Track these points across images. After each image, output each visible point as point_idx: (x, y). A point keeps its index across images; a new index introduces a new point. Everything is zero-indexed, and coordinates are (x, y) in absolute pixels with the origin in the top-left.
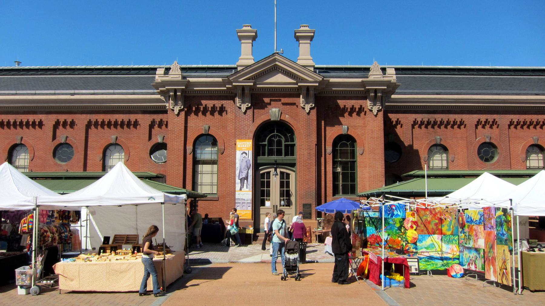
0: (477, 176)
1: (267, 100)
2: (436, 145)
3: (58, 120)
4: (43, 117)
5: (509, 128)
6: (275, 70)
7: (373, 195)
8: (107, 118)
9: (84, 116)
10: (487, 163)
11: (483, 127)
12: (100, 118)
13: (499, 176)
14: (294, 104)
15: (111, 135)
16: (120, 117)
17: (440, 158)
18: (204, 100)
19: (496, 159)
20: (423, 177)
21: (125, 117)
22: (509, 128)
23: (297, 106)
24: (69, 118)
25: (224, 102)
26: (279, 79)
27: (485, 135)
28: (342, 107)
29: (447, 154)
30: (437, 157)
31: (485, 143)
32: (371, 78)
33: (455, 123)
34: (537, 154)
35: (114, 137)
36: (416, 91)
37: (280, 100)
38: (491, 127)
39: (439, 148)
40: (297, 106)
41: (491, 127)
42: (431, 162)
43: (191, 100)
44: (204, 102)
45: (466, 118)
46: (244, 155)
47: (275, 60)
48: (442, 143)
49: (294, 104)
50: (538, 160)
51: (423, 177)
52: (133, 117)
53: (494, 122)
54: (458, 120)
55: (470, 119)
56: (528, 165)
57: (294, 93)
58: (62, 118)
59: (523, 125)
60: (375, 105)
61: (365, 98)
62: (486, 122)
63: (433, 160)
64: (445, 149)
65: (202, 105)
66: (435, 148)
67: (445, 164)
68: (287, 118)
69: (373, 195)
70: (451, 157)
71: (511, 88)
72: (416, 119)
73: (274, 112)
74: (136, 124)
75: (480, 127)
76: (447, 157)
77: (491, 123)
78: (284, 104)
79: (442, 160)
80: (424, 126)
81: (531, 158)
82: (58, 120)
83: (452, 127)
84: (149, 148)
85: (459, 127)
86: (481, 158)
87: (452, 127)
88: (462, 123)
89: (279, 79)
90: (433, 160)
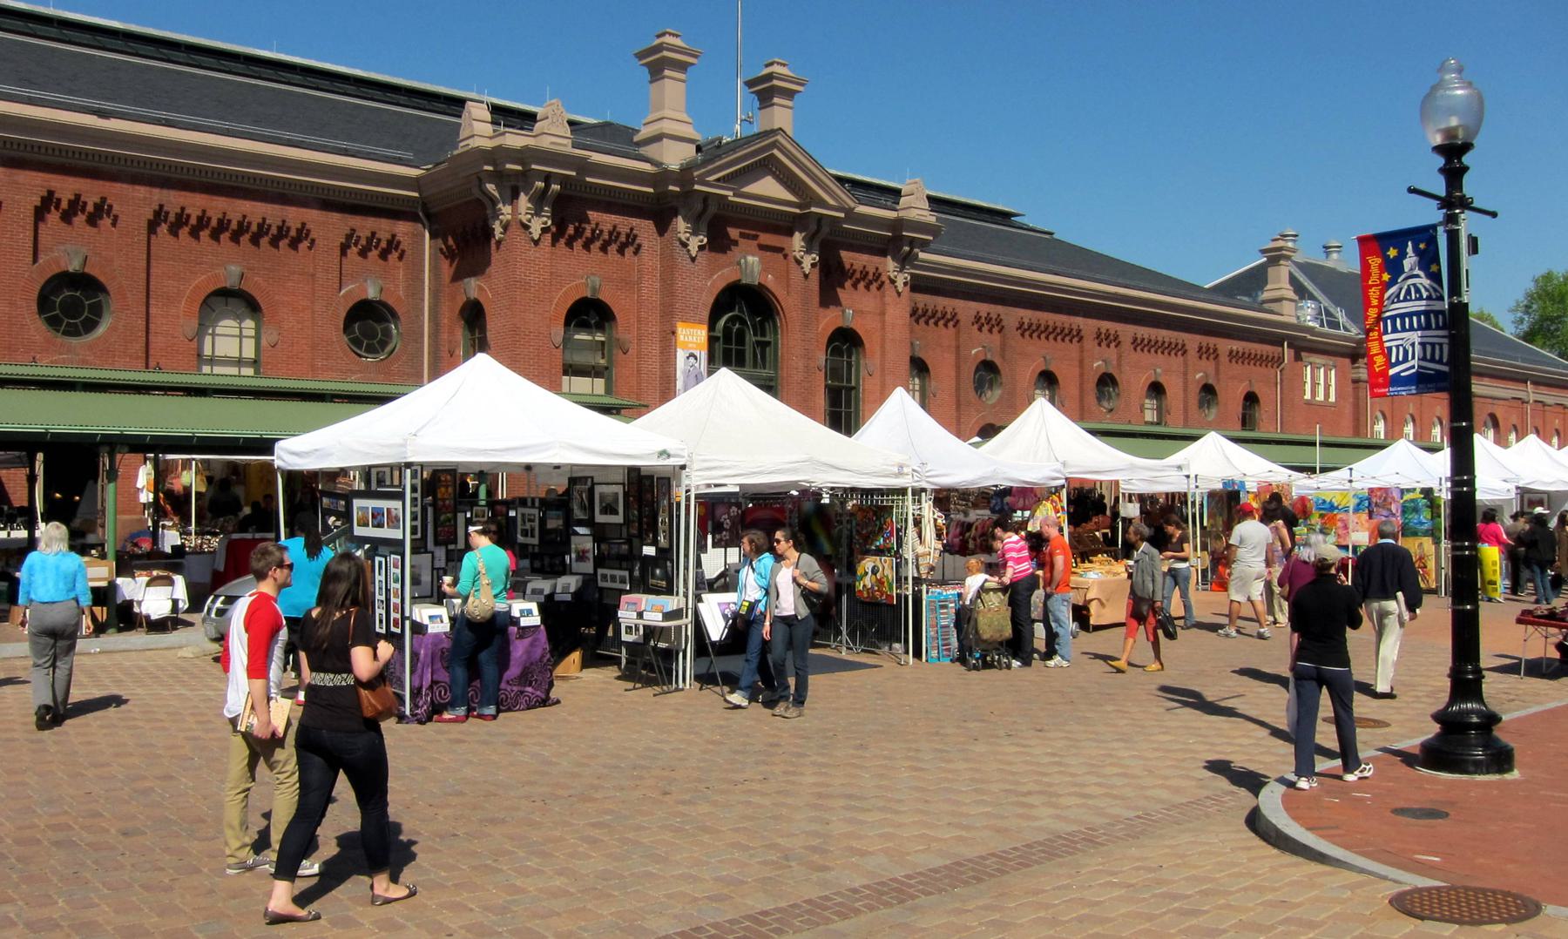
0: (1194, 438)
1: (734, 233)
2: (224, 294)
3: (51, 193)
4: (313, 216)
6: (768, 167)
8: (217, 206)
9: (141, 191)
10: (74, 341)
11: (363, 253)
12: (195, 203)
13: (1094, 432)
14: (779, 250)
15: (229, 265)
16: (255, 211)
17: (237, 332)
18: (597, 210)
19: (101, 330)
20: (1314, 444)
21: (272, 213)
23: (785, 256)
24: (91, 190)
25: (635, 222)
26: (768, 188)
27: (69, 249)
28: (847, 266)
29: (922, 379)
30: (227, 326)
32: (545, 143)
33: (282, 231)
35: (235, 269)
36: (287, 135)
37: (755, 237)
40: (785, 256)
42: (208, 340)
43: (573, 206)
44: (593, 215)
45: (118, 193)
46: (692, 360)
47: (774, 145)
48: (244, 287)
49: (779, 250)
51: (1314, 444)
52: (294, 216)
54: (294, 225)
55: (966, 309)
56: (207, 351)
57: (783, 225)
58: (66, 187)
60: (538, 213)
61: (883, 253)
64: (252, 306)
65: (589, 222)
66: (222, 299)
67: (249, 352)
68: (769, 280)
72: (183, 209)
73: (751, 264)
74: (300, 237)
75: (53, 217)
76: (258, 330)
78: (762, 247)
79: (241, 336)
80: (286, 241)
81: (218, 330)
82: (51, 193)
83: (195, 233)
84: (344, 314)
86: (53, 322)
87: (195, 233)
88: (302, 234)
89: (768, 188)
90: (214, 335)
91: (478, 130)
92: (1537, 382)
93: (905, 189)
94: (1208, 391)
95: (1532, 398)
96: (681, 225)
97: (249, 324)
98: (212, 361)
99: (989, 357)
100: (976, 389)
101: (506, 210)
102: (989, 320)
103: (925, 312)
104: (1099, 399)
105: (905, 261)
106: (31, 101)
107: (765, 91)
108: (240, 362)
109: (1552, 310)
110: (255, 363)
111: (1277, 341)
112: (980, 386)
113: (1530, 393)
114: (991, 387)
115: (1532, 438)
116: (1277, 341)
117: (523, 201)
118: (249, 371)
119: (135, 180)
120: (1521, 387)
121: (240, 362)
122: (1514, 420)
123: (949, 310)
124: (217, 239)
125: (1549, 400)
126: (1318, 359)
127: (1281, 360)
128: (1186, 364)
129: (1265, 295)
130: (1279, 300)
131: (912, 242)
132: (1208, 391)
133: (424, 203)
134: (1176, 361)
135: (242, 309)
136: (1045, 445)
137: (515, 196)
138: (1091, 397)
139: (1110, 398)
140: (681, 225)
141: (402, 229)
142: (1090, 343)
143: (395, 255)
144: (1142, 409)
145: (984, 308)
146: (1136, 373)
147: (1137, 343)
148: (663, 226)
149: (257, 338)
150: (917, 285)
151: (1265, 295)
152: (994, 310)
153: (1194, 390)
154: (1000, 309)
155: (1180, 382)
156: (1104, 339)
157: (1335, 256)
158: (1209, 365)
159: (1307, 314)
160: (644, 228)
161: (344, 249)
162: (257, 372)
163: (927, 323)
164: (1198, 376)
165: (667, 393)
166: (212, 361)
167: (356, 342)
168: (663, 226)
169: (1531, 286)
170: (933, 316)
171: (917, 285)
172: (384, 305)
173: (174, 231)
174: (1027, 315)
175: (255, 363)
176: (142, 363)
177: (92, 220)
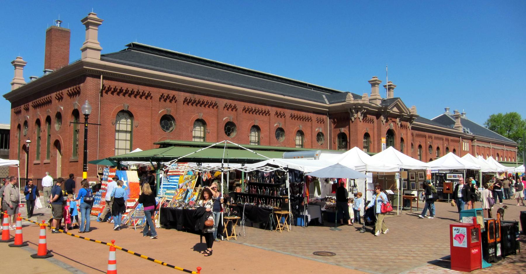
2: (123, 111)
5: (160, 101)
7: (38, 149)
9: (182, 94)
14: (394, 122)
16: (131, 87)
22: (160, 101)
30: (123, 121)
31: (279, 128)
34: (126, 119)
35: (126, 105)
38: (171, 101)
39: (125, 114)
41: (171, 101)
42: (118, 125)
44: (368, 116)
47: (398, 101)
50: (127, 124)
53: (149, 95)
56: (194, 135)
59: (115, 91)
61: (407, 121)
62: (168, 97)
63: (119, 124)
64: (130, 115)
69: (38, 149)
70: (135, 122)
71: (186, 71)
73: (392, 126)
74: (148, 96)
77: (171, 98)
81: (121, 122)
83: (141, 97)
85: (146, 98)
88: (174, 98)
90: (119, 124)
91: (350, 100)
92: (507, 145)
93: (363, 96)
94: (447, 148)
95: (492, 147)
96: (382, 118)
97: (129, 120)
98: (194, 137)
99: (280, 126)
100: (277, 137)
101: (356, 115)
102: (280, 114)
103: (248, 109)
104: (318, 141)
105: (411, 123)
106: (134, 66)
107: (390, 88)
108: (200, 138)
109: (494, 124)
110: (204, 138)
111: (459, 137)
112: (278, 136)
113: (505, 148)
114: (282, 136)
115: (491, 158)
116: (459, 137)
117: (359, 113)
118: (256, 144)
119: (288, 108)
120: (488, 144)
121: (200, 138)
122: (488, 153)
123: (282, 113)
124: (125, 96)
125: (508, 150)
126: (465, 141)
127: (459, 141)
128: (426, 140)
129: (455, 126)
130: (459, 127)
131: (413, 119)
132: (430, 147)
133: (328, 112)
134: (265, 118)
135: (201, 124)
136: (391, 160)
137: (357, 112)
138: (273, 136)
139: (321, 140)
140: (382, 118)
141: (324, 117)
142: (315, 123)
143: (174, 101)
144: (295, 141)
145: (279, 110)
146: (244, 123)
147: (245, 110)
148: (378, 118)
149: (132, 125)
150: (413, 128)
151: (455, 126)
152: (233, 103)
153: (445, 149)
154: (235, 102)
155: (425, 144)
156: (430, 137)
157: (448, 111)
158: (430, 140)
159: (461, 130)
160: (374, 118)
161: (160, 99)
162: (204, 141)
163: (253, 113)
164: (316, 130)
165: (379, 150)
166: (194, 137)
167: (163, 127)
168: (378, 118)
169: (489, 118)
170: (248, 110)
171: (413, 128)
172: (170, 115)
173: (112, 93)
174: (188, 95)
175: (204, 138)
176: (310, 146)
177: (146, 98)
